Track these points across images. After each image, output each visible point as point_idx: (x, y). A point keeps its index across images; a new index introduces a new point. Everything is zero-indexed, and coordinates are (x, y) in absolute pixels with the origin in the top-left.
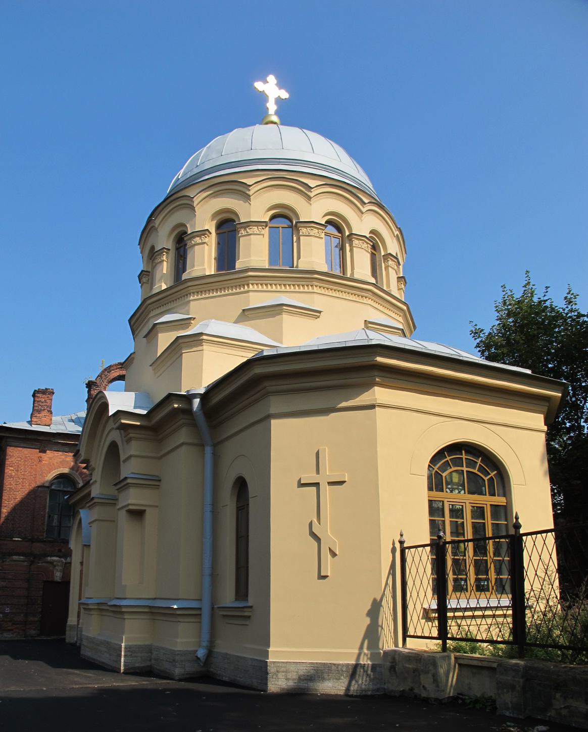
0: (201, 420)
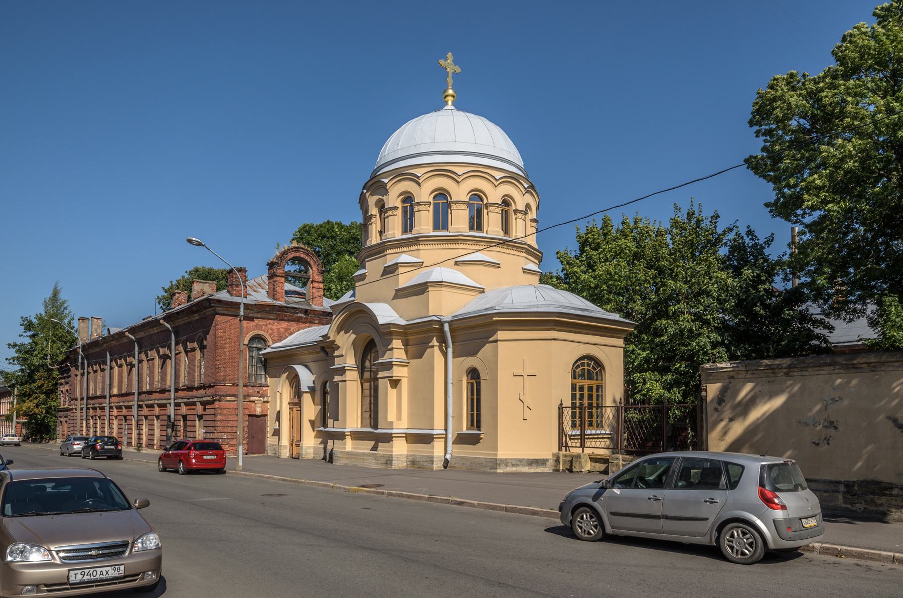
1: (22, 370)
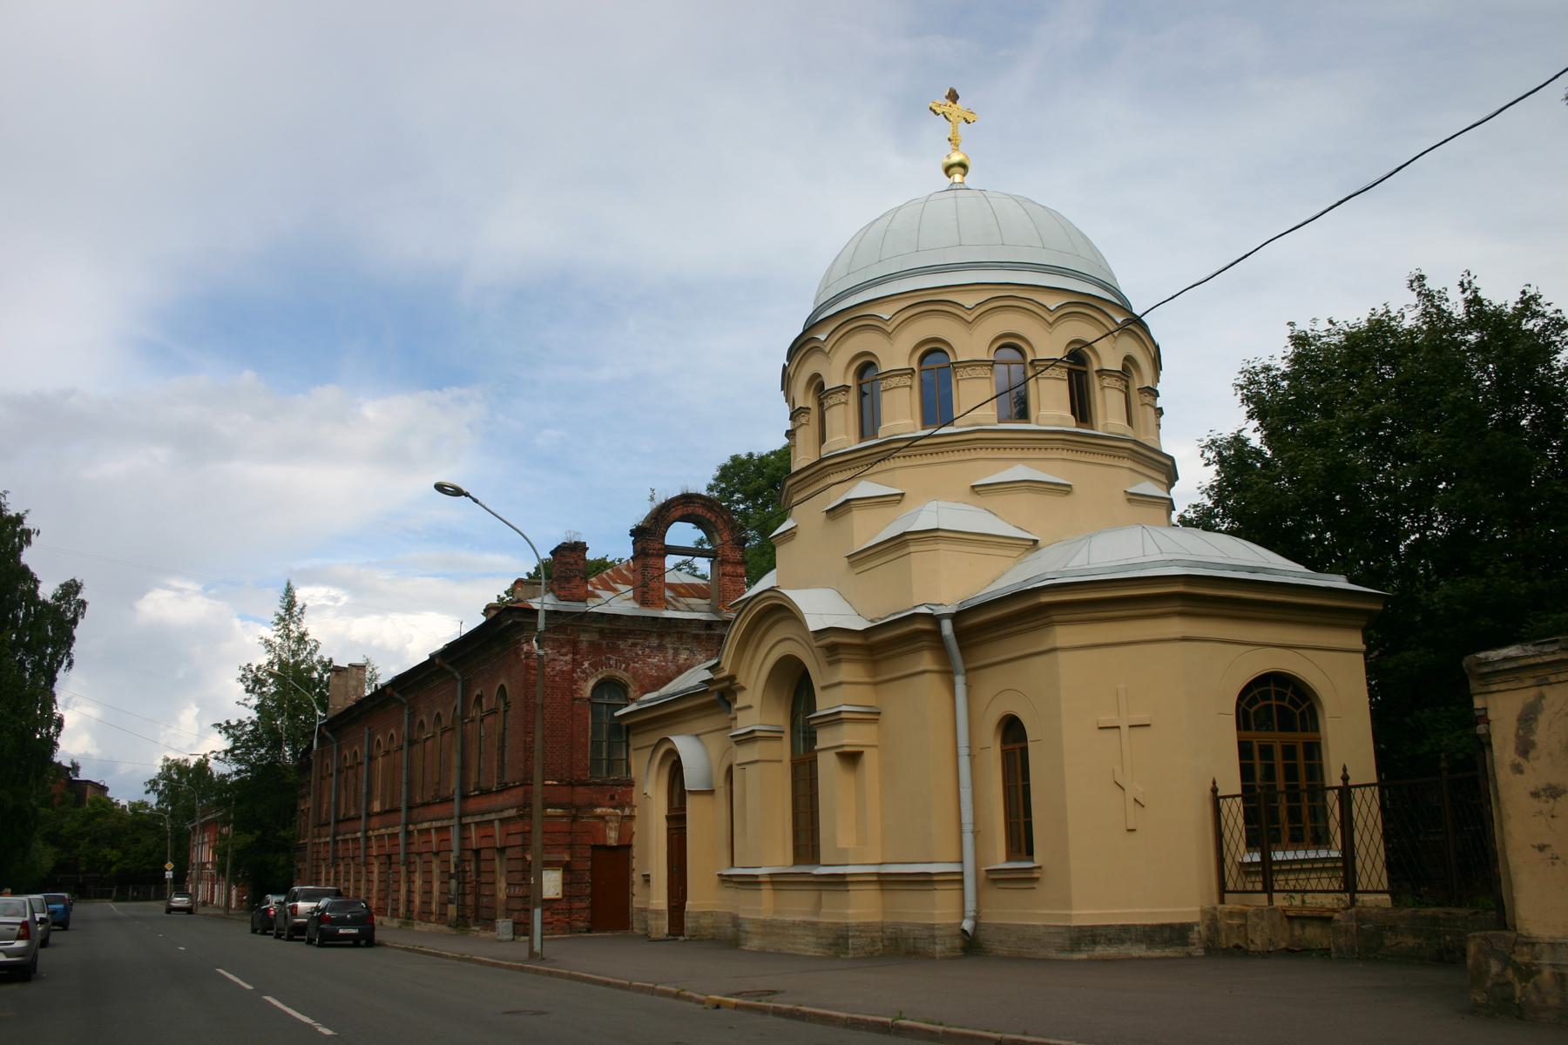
0: (953, 645)
1: (238, 772)
